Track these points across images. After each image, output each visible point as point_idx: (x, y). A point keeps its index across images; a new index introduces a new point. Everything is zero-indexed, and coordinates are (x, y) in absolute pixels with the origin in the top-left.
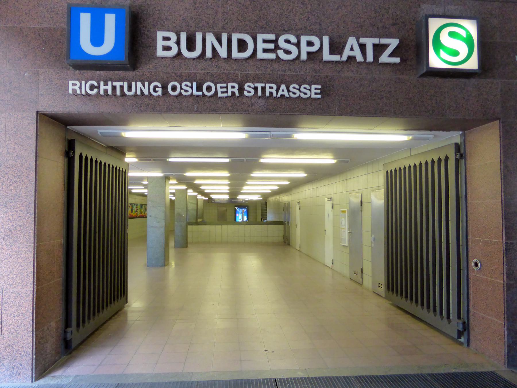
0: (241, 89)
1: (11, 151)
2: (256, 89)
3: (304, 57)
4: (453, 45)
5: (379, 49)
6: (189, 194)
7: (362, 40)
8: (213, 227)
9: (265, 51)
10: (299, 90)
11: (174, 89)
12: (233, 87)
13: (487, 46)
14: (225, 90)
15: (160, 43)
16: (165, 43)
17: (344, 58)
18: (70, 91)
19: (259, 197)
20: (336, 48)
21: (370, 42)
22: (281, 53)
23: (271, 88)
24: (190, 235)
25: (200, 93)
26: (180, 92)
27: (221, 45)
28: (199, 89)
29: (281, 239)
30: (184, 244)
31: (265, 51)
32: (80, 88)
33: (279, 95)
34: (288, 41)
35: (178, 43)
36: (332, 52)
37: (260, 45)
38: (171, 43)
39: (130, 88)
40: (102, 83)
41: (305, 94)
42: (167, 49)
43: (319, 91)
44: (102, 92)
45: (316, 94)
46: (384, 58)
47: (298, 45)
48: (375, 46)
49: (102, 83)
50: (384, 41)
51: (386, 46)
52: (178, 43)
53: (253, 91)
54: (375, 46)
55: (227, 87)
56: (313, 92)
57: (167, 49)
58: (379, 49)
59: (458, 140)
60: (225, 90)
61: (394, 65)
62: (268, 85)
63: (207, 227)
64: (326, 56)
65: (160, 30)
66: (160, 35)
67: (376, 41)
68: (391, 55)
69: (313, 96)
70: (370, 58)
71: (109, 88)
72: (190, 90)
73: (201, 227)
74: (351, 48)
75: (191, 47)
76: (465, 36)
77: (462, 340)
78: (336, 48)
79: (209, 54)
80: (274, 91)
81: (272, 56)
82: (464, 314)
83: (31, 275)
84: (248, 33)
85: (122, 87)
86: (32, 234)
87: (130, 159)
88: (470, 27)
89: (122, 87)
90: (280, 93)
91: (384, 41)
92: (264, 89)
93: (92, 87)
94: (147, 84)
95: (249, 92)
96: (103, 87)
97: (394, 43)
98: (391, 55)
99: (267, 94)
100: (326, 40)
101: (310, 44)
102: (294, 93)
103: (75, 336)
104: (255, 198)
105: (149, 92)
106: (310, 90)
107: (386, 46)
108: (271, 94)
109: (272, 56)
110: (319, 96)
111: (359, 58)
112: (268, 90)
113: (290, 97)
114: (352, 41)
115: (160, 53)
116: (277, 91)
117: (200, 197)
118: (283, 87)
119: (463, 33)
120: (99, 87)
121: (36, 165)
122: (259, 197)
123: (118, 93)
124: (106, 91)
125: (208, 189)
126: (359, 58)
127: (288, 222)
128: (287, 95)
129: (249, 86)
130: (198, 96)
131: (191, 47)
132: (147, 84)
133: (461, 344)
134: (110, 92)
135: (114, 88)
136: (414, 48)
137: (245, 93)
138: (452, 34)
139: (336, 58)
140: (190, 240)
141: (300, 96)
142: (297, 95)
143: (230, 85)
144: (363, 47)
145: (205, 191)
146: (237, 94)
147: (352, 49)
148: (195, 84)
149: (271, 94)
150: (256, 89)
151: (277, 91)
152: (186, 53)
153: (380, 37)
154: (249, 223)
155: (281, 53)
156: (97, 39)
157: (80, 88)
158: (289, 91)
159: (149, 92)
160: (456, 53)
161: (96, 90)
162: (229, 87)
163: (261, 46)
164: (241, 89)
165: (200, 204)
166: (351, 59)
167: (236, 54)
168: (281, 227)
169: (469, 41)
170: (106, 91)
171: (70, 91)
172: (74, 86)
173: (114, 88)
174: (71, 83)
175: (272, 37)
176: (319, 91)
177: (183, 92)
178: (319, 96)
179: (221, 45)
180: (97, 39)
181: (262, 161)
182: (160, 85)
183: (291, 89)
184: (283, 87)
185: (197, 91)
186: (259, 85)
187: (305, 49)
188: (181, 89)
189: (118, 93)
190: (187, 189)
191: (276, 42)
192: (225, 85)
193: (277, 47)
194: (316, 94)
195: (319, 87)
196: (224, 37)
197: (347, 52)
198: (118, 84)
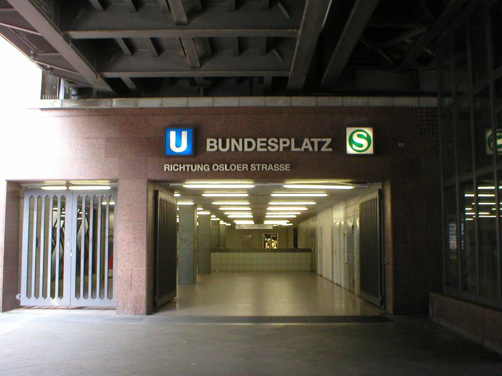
0: (249, 167)
1: (135, 199)
2: (257, 167)
3: (281, 150)
4: (360, 141)
5: (321, 144)
6: (212, 219)
7: (312, 140)
8: (236, 254)
9: (262, 147)
10: (279, 167)
11: (216, 167)
12: (245, 166)
13: (378, 141)
14: (241, 167)
15: (208, 145)
16: (212, 145)
17: (303, 149)
18: (165, 170)
19: (288, 223)
20: (298, 144)
21: (316, 141)
22: (269, 148)
23: (264, 167)
24: (212, 261)
25: (228, 170)
26: (219, 170)
27: (239, 145)
28: (228, 167)
29: (309, 268)
30: (207, 270)
31: (262, 147)
32: (170, 168)
33: (268, 170)
34: (273, 142)
35: (217, 144)
36: (296, 147)
37: (259, 145)
38: (214, 144)
39: (194, 168)
40: (180, 165)
41: (282, 169)
42: (212, 147)
43: (289, 167)
44: (180, 170)
45: (288, 169)
46: (324, 149)
47: (278, 144)
48: (319, 142)
49: (180, 165)
50: (323, 140)
51: (325, 142)
52: (217, 144)
53: (255, 168)
54: (319, 142)
55: (242, 166)
56: (286, 168)
57: (212, 147)
58: (321, 144)
59: (380, 187)
60: (241, 167)
61: (329, 152)
62: (263, 165)
63: (230, 255)
64: (293, 149)
65: (209, 138)
66: (208, 140)
67: (319, 140)
68: (328, 147)
69: (286, 170)
70: (316, 149)
71: (184, 168)
72: (224, 168)
73: (224, 254)
74: (306, 144)
75: (224, 146)
76: (353, 145)
77: (383, 307)
78: (298, 144)
79: (233, 149)
80: (266, 168)
81: (265, 150)
82: (383, 293)
83: (145, 261)
84: (253, 138)
85: (190, 167)
86: (145, 241)
87: (177, 195)
88: (369, 132)
89: (190, 167)
90: (269, 168)
91: (323, 140)
92: (261, 167)
93: (176, 168)
94: (202, 165)
95: (253, 169)
96: (180, 167)
97: (329, 141)
98: (328, 147)
99: (263, 170)
100: (293, 140)
101: (285, 143)
102: (276, 169)
103: (159, 302)
104: (284, 223)
105: (203, 169)
106: (285, 167)
107: (325, 142)
108: (264, 169)
109: (265, 150)
110: (289, 170)
111: (311, 149)
112: (263, 168)
113: (274, 170)
114: (306, 140)
115: (208, 149)
116: (268, 168)
117: (222, 222)
118: (270, 165)
119: (365, 135)
120: (179, 167)
121: (147, 206)
122: (288, 223)
123: (188, 170)
124: (182, 169)
125: (231, 215)
126: (311, 149)
127: (314, 250)
128: (273, 170)
129: (253, 166)
130: (227, 171)
131: (224, 146)
132: (202, 165)
133: (382, 309)
134: (184, 170)
135: (186, 167)
136: (339, 143)
137: (251, 169)
138: (359, 136)
139: (298, 149)
140: (212, 268)
141: (279, 170)
142: (278, 170)
143: (243, 165)
144: (312, 144)
145: (229, 217)
146: (247, 169)
147: (307, 145)
148: (226, 165)
149: (264, 169)
150: (257, 167)
151: (268, 168)
152: (221, 149)
153: (321, 138)
154: (278, 250)
155: (269, 148)
156: (178, 145)
157: (170, 168)
158: (274, 168)
159: (203, 169)
160: (361, 146)
161: (178, 169)
162: (243, 166)
163: (259, 144)
164: (249, 167)
165: (222, 230)
166: (306, 150)
167: (246, 149)
168: (308, 254)
169: (368, 139)
170: (182, 169)
171: (165, 170)
172: (166, 167)
173: (186, 167)
174: (165, 165)
175: (265, 140)
176: (289, 167)
177: (220, 169)
178: (289, 170)
179: (239, 145)
180: (178, 145)
181: (272, 195)
182: (208, 166)
183: (275, 166)
184: (270, 165)
185: (227, 168)
186: (259, 165)
187: (282, 145)
188: (219, 167)
189: (188, 170)
190: (210, 215)
191: (267, 142)
192: (241, 165)
193: (268, 145)
194: (288, 169)
195: (289, 165)
196: (241, 140)
197: (304, 147)
198: (188, 166)
